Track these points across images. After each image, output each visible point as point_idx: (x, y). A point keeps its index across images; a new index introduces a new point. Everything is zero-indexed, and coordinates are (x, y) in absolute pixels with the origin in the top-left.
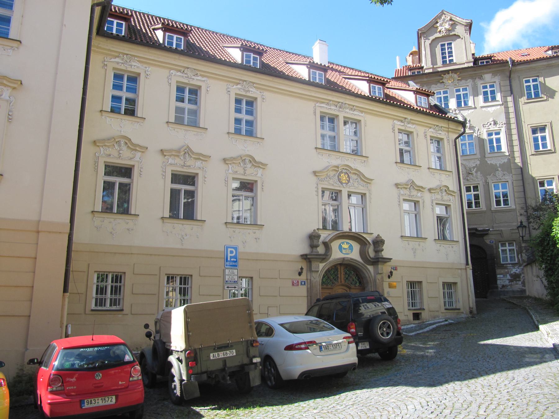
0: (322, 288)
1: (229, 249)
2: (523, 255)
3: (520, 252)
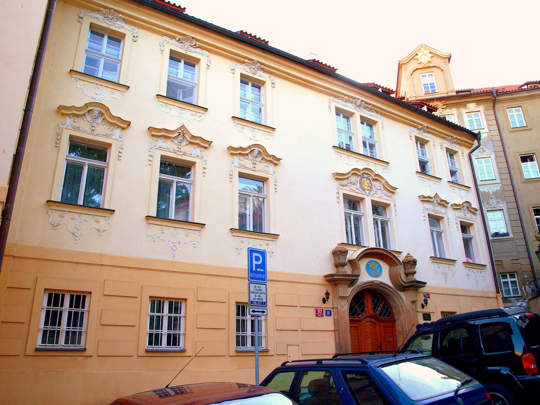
0: (351, 321)
1: (254, 254)
2: (527, 287)
3: (523, 283)
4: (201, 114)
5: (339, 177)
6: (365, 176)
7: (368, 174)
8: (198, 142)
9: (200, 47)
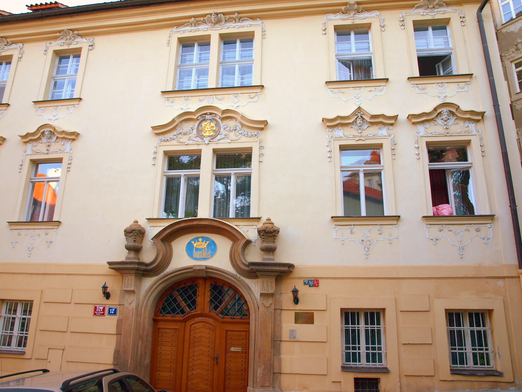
4: (382, 87)
5: (334, 123)
6: (207, 117)
7: (211, 114)
8: (381, 120)
9: (13, 43)
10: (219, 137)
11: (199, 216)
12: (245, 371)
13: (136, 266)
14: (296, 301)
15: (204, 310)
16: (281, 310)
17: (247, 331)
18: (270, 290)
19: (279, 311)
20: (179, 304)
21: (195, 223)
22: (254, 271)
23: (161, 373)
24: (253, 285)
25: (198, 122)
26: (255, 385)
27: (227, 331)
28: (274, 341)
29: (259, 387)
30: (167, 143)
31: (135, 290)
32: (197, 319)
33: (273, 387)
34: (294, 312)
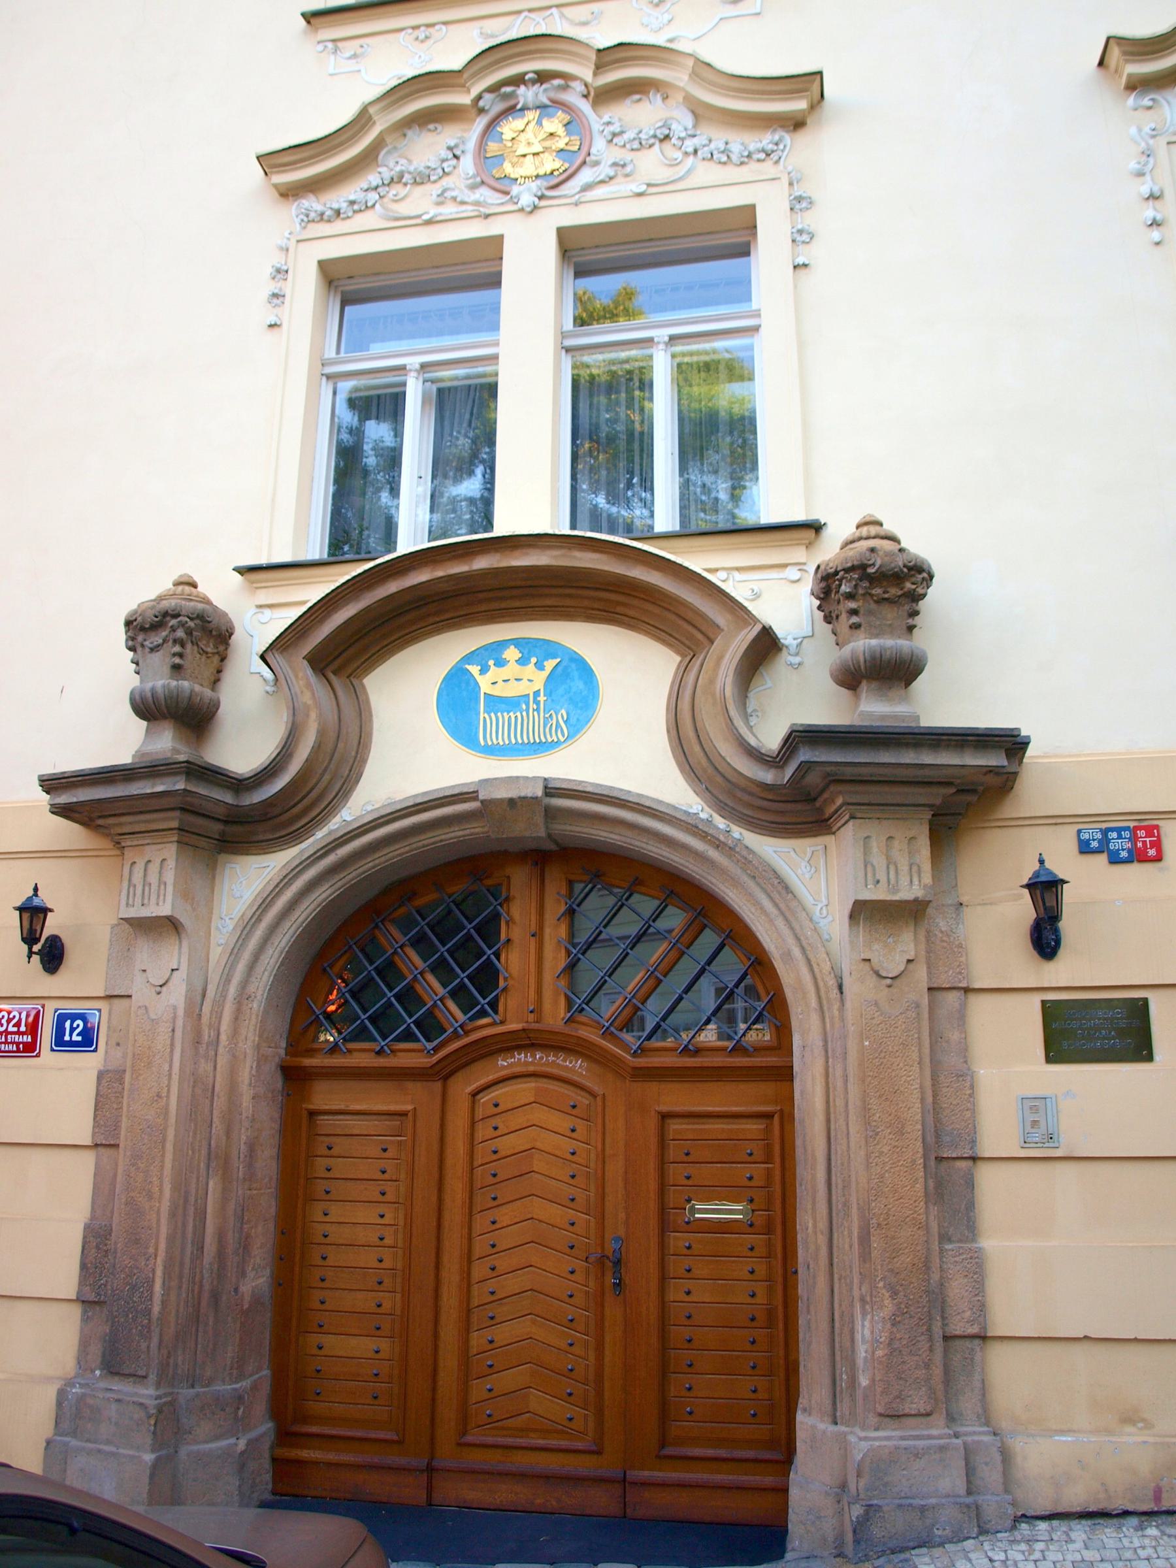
6: (526, 94)
7: (542, 77)
10: (586, 176)
11: (502, 527)
12: (770, 1322)
13: (180, 784)
14: (1045, 939)
15: (537, 1011)
16: (967, 990)
17: (768, 1116)
18: (904, 881)
19: (952, 998)
20: (430, 1013)
21: (482, 563)
22: (808, 789)
23: (328, 1341)
24: (804, 869)
25: (481, 122)
26: (844, 1408)
27: (665, 1117)
28: (940, 1159)
29: (873, 1420)
30: (339, 226)
31: (183, 919)
32: (505, 1063)
33: (951, 1418)
34: (1036, 1000)
